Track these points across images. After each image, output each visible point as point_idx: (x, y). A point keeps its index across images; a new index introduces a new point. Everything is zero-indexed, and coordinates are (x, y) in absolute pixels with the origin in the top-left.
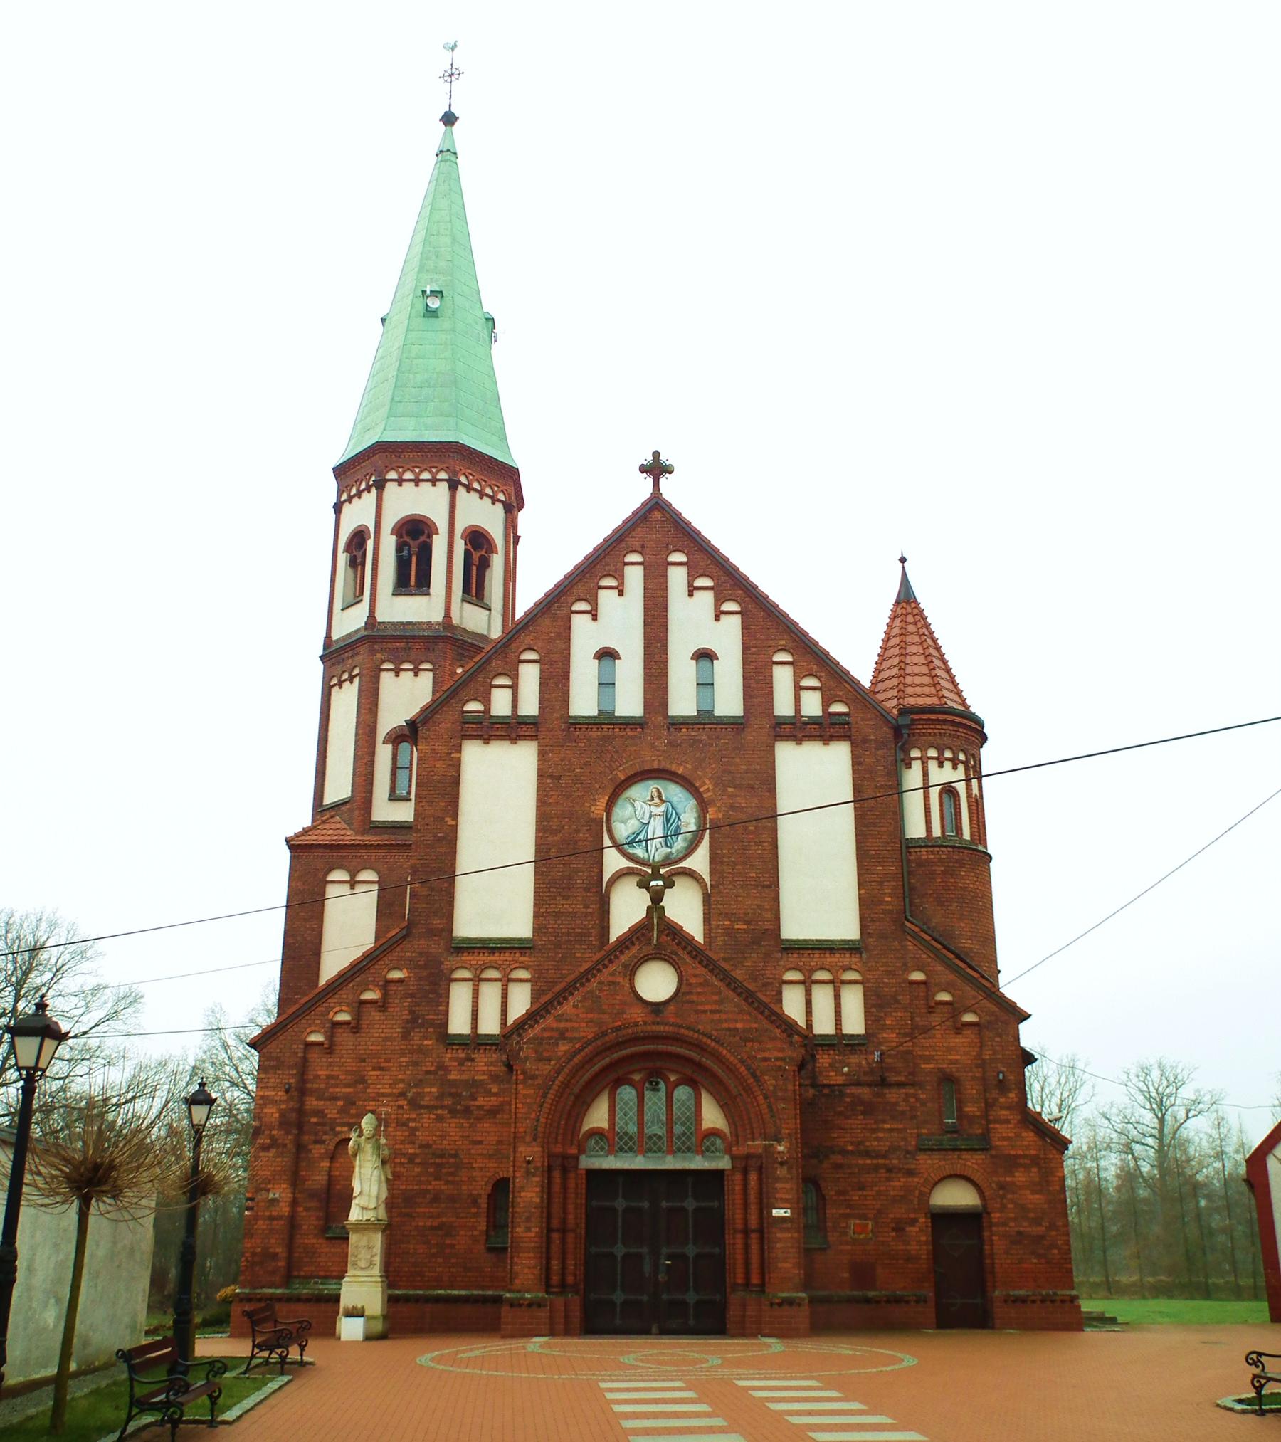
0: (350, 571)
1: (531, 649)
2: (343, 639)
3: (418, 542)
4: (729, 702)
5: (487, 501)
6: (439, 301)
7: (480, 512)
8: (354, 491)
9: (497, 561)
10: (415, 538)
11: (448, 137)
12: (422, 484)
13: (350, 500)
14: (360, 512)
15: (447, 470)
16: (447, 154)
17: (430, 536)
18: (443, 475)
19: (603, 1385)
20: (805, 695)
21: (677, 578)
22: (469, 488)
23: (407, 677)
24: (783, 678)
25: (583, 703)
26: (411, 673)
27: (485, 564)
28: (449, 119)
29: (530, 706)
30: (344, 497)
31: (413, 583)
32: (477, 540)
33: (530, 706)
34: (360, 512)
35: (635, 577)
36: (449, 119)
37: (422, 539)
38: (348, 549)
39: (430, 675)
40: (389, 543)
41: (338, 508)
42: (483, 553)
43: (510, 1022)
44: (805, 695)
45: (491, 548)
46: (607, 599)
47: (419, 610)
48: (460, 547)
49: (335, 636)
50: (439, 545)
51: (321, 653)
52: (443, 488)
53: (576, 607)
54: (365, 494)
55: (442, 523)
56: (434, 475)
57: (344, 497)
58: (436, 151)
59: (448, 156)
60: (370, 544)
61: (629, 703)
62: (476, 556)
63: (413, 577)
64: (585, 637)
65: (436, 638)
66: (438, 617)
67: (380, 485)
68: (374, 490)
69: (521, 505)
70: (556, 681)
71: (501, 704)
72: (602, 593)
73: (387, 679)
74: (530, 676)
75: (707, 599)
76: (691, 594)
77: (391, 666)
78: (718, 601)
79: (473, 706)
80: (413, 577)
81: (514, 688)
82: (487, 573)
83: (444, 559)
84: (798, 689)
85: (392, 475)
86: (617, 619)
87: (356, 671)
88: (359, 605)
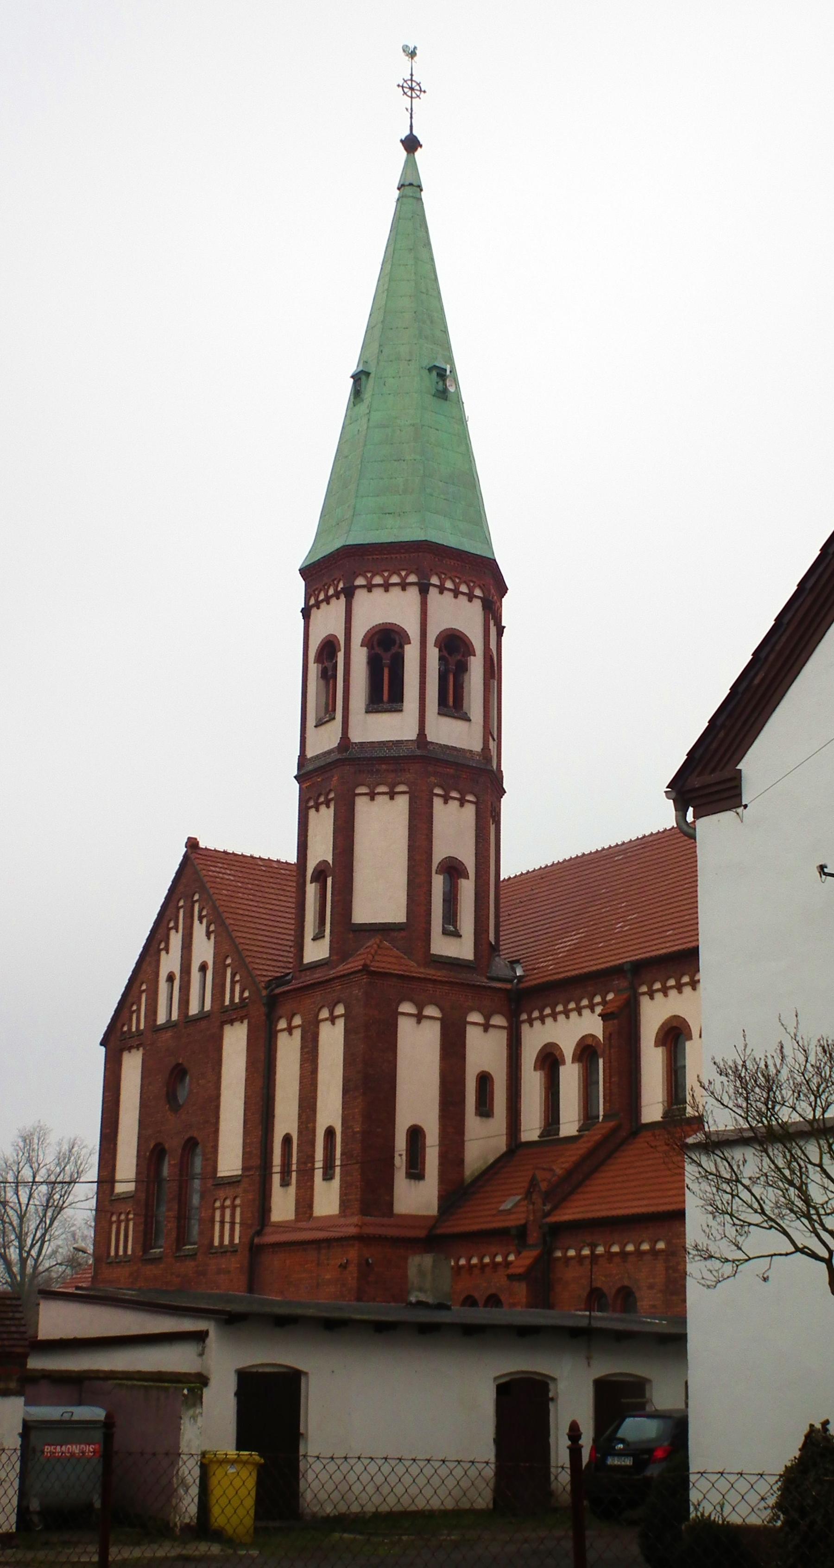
0: (322, 682)
2: (317, 757)
3: (389, 654)
5: (463, 599)
6: (407, 374)
7: (457, 613)
8: (322, 597)
9: (476, 665)
10: (387, 649)
11: (411, 166)
12: (392, 589)
13: (317, 605)
14: (330, 620)
15: (417, 572)
17: (402, 647)
18: (412, 578)
19: (227, 1003)
22: (442, 589)
23: (454, 805)
27: (462, 668)
28: (411, 144)
30: (312, 602)
31: (386, 697)
32: (453, 645)
34: (330, 620)
37: (394, 650)
38: (319, 659)
40: (360, 657)
41: (306, 613)
42: (459, 657)
43: (687, 1190)
45: (469, 650)
47: (394, 728)
48: (433, 654)
49: (310, 754)
50: (411, 654)
51: (295, 773)
52: (413, 594)
53: (358, 791)
54: (334, 601)
55: (412, 629)
56: (404, 579)
57: (312, 602)
58: (396, 185)
60: (341, 656)
62: (452, 660)
63: (385, 693)
65: (411, 759)
67: (349, 593)
68: (343, 599)
69: (502, 589)
73: (362, 805)
80: (385, 693)
82: (466, 677)
83: (418, 667)
85: (360, 581)
87: (332, 795)
88: (321, 941)
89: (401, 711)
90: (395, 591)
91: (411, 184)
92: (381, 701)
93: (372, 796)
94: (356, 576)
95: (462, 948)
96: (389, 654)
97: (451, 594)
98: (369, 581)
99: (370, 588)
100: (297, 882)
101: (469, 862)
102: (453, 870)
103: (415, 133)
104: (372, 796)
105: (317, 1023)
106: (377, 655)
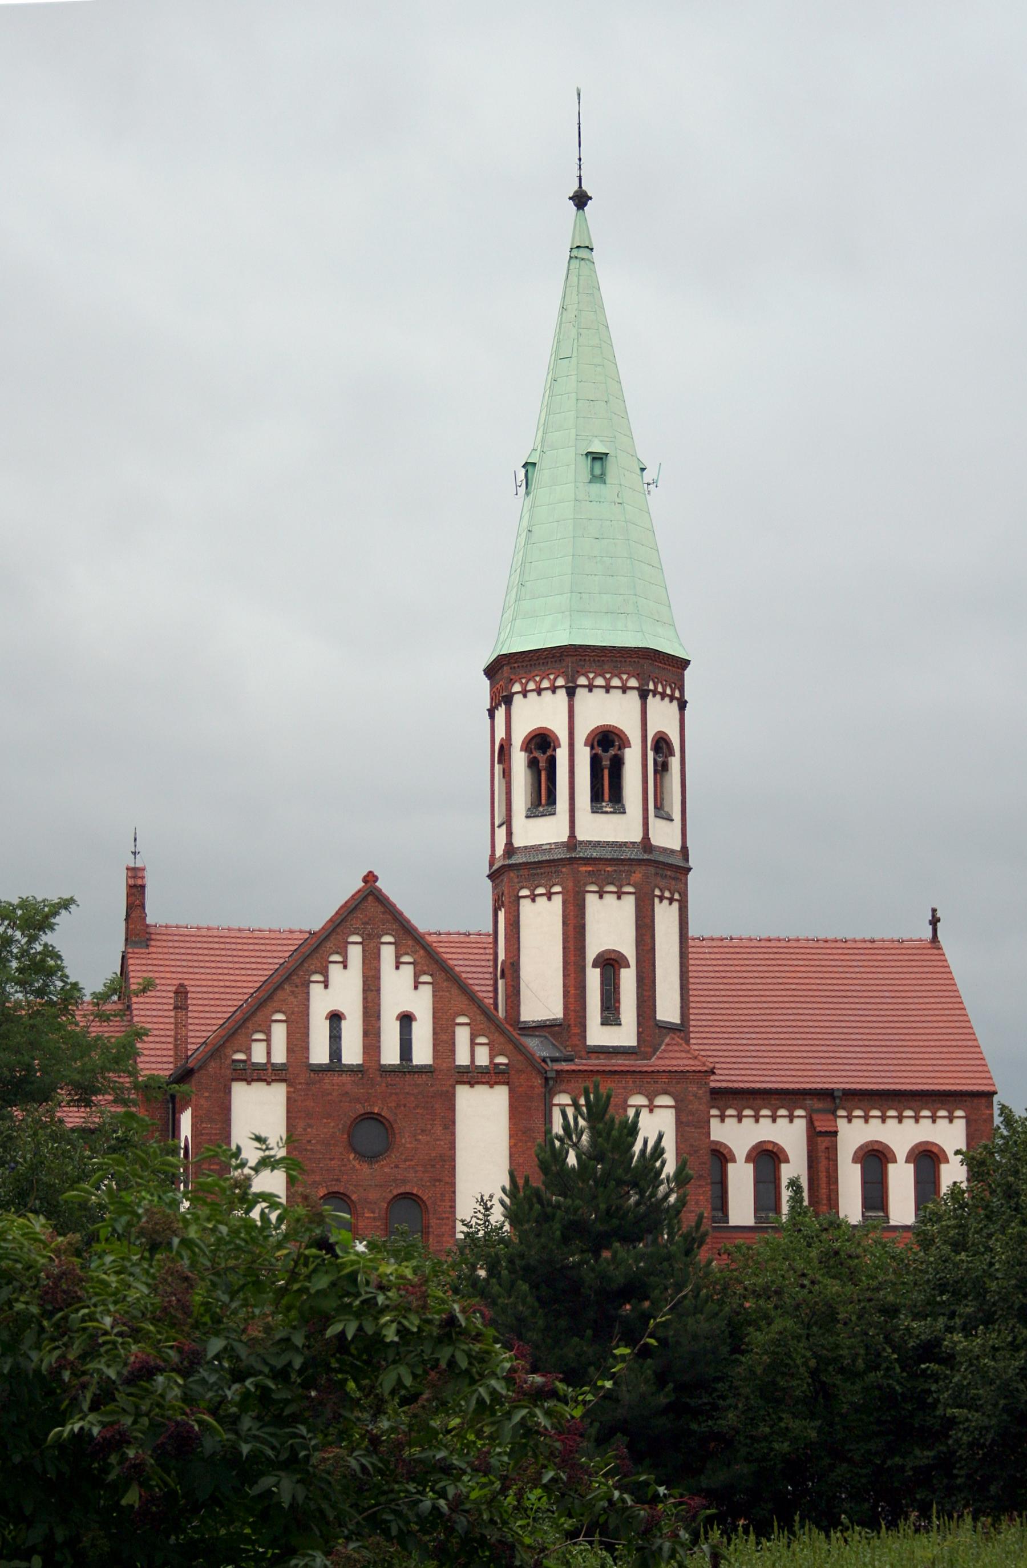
1: (279, 1012)
4: (422, 1055)
11: (581, 226)
15: (638, 676)
16: (581, 251)
17: (555, 750)
20: (478, 1049)
21: (388, 953)
23: (610, 899)
24: (462, 1035)
25: (319, 1054)
26: (615, 896)
27: (617, 765)
29: (280, 1056)
32: (662, 745)
33: (280, 1056)
35: (355, 953)
36: (581, 200)
37: (612, 752)
39: (411, 967)
44: (478, 1049)
46: (335, 970)
50: (632, 758)
52: (634, 697)
53: (589, 888)
59: (583, 253)
61: (352, 1054)
64: (321, 1002)
66: (637, 837)
70: (298, 1040)
71: (258, 1054)
72: (331, 967)
73: (591, 900)
74: (279, 1033)
75: (408, 971)
76: (397, 968)
77: (595, 888)
78: (416, 976)
79: (240, 1056)
81: (268, 1041)
83: (574, 769)
84: (473, 1044)
85: (582, 681)
86: (339, 990)
89: (554, 814)
90: (547, 695)
91: (578, 247)
92: (539, 804)
93: (533, 898)
94: (579, 673)
95: (625, 1035)
96: (545, 757)
97: (549, 692)
98: (608, 681)
99: (590, 688)
100: (688, 959)
101: (630, 952)
102: (610, 964)
103: (584, 187)
104: (533, 898)
105: (276, 1161)
106: (535, 758)
